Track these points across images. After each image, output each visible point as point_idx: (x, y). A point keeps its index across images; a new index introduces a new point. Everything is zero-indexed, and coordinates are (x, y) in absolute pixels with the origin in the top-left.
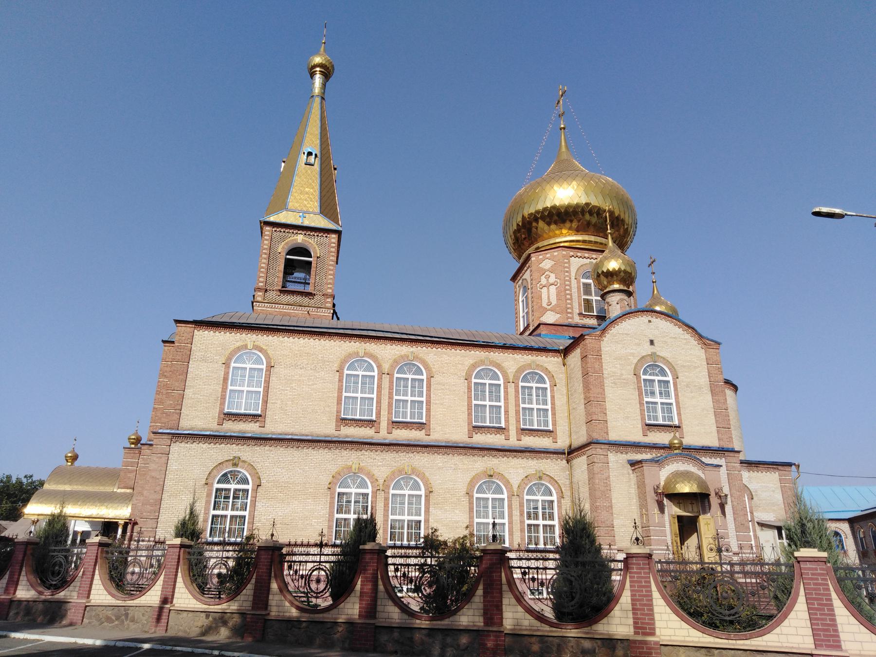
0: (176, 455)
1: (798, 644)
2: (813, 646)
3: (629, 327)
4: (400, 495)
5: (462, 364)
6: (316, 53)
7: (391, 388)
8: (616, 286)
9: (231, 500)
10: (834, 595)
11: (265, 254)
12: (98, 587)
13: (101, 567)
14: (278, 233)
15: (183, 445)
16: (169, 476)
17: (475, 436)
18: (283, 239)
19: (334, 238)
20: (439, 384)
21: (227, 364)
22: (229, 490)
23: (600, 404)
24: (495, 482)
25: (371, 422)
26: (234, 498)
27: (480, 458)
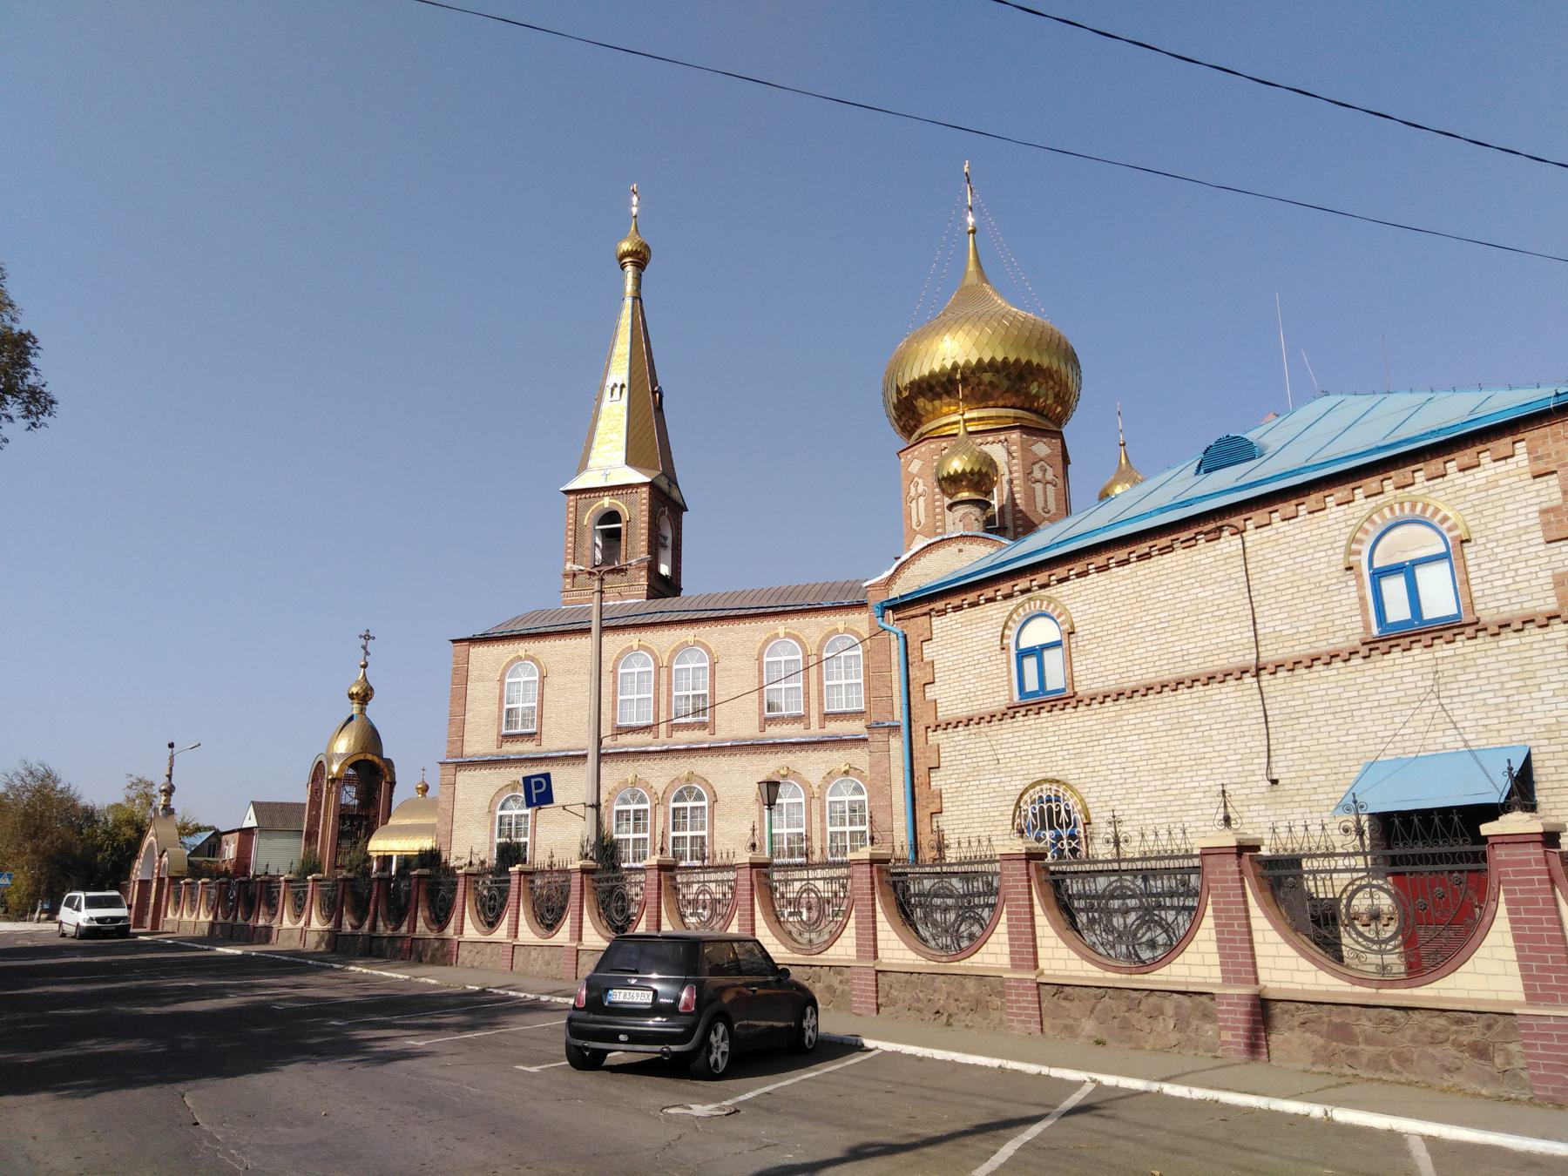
0: (461, 785)
1: (1302, 984)
2: (1521, 997)
3: (929, 564)
4: (840, 802)
5: (751, 641)
6: (624, 238)
7: (669, 684)
8: (965, 495)
9: (688, 819)
10: (1255, 911)
11: (571, 530)
12: (996, 949)
13: (525, 901)
14: (583, 500)
15: (467, 773)
16: (457, 806)
17: (767, 728)
18: (588, 506)
19: (644, 492)
20: (724, 670)
21: (502, 681)
22: (628, 811)
23: (883, 676)
24: (790, 783)
25: (531, 735)
26: (636, 819)
27: (772, 756)
